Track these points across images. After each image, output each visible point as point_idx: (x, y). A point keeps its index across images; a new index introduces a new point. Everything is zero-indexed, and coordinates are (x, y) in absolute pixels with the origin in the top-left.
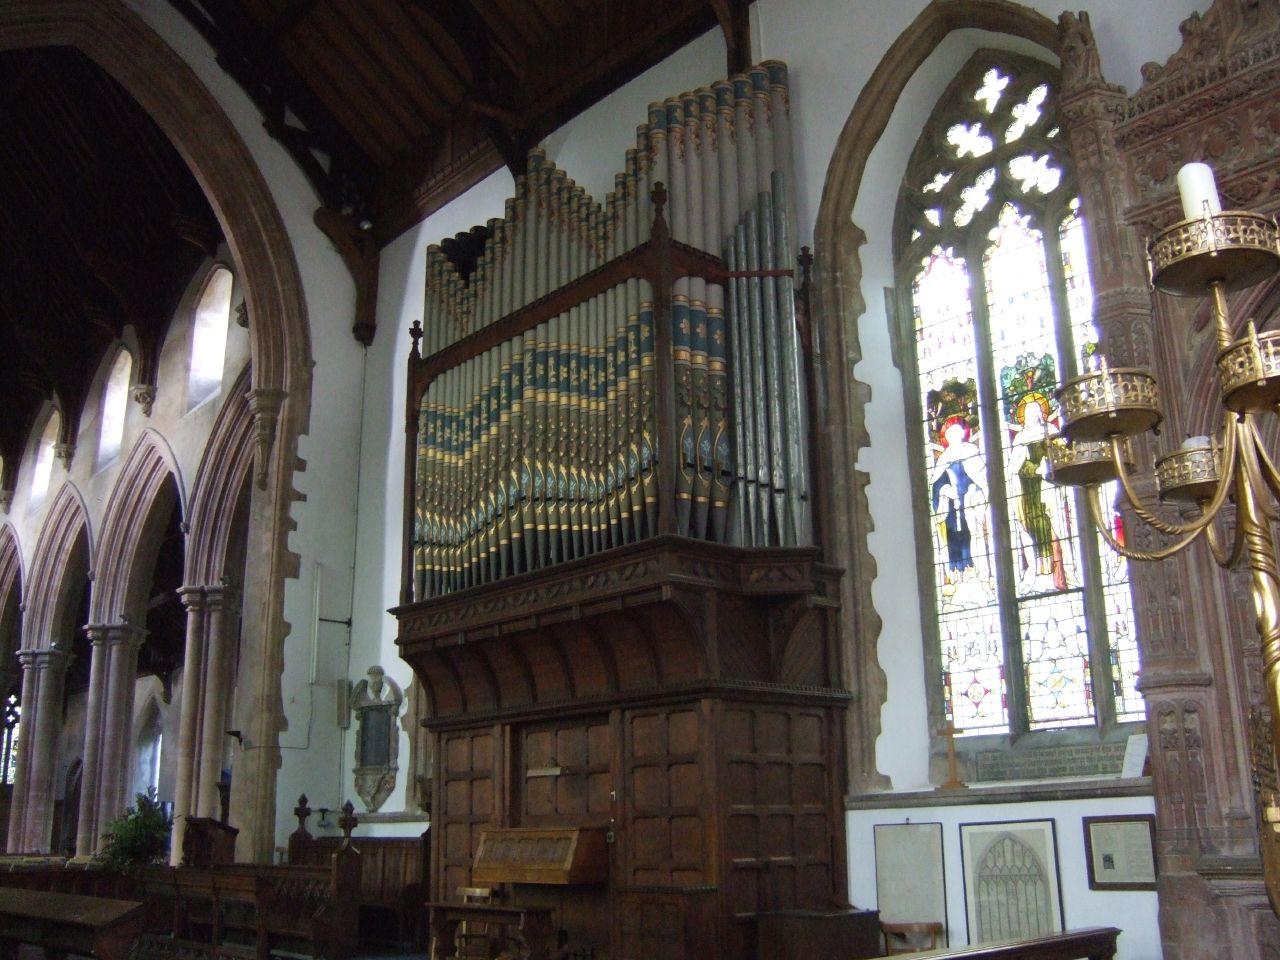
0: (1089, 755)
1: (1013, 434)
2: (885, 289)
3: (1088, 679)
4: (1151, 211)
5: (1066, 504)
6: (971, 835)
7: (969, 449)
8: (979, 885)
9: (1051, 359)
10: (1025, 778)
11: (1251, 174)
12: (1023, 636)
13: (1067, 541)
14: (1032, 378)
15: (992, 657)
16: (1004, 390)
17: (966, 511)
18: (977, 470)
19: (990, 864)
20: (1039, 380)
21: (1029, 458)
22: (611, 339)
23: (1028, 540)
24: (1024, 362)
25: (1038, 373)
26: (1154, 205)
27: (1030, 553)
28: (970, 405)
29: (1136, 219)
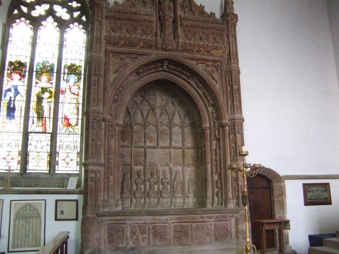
1: (37, 83)
2: (3, 23)
3: (49, 159)
4: (110, 38)
5: (50, 108)
6: (15, 204)
7: (20, 83)
8: (16, 220)
9: (54, 65)
10: (25, 187)
11: (138, 41)
12: (29, 144)
13: (48, 118)
14: (47, 69)
15: (16, 148)
16: (37, 69)
17: (15, 102)
18: (23, 90)
19: (21, 213)
20: (49, 70)
21: (41, 91)
23: (36, 115)
24: (45, 63)
25: (49, 68)
26: (112, 37)
27: (35, 119)
28: (24, 70)
29: (106, 39)
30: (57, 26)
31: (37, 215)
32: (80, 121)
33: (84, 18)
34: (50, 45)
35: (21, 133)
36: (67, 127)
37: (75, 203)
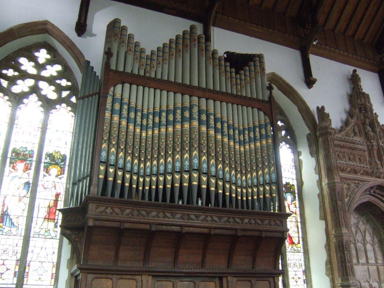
22: (145, 111)
30: (41, 106)
32: (301, 239)
33: (74, 99)
34: (63, 132)
36: (292, 245)
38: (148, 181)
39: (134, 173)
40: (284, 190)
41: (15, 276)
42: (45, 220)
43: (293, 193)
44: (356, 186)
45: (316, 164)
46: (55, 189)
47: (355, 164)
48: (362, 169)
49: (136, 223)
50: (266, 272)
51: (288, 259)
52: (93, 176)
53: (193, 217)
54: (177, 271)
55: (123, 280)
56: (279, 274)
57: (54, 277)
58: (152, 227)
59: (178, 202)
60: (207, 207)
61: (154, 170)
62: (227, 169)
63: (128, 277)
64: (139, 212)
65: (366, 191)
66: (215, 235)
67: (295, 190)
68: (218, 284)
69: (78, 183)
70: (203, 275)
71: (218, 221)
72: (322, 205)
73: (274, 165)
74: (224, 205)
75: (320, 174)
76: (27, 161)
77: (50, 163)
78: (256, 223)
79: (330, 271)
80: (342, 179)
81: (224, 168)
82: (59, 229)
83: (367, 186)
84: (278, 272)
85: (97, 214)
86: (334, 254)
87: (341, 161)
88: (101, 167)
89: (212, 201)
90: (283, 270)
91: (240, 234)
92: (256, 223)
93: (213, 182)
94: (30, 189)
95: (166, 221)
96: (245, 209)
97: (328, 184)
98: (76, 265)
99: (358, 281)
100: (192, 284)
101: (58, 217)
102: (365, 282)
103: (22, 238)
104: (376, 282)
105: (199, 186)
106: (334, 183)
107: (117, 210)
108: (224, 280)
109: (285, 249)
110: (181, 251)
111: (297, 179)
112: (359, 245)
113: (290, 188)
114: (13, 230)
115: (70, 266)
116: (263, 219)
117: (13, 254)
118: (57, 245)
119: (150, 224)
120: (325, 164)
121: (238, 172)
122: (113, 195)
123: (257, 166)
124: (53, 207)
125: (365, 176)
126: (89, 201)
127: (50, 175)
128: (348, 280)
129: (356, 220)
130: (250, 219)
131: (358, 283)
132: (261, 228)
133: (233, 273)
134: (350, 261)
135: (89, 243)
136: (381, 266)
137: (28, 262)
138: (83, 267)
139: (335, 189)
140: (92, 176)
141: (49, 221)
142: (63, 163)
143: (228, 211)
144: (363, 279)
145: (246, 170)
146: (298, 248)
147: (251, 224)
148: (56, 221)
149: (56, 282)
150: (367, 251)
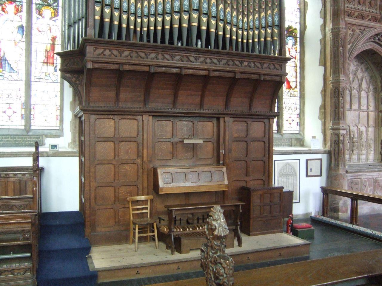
0: (23, 139)
6: (278, 163)
19: (283, 171)
31: (294, 173)
32: (298, 84)
35: (57, 83)
36: (289, 90)
37: (319, 161)
38: (146, 21)
39: (131, 14)
40: (286, 33)
41: (22, 118)
42: (44, 64)
43: (295, 37)
44: (361, 32)
45: (322, 7)
46: (51, 32)
47: (364, 8)
48: (370, 14)
49: (135, 65)
50: (263, 114)
51: (284, 103)
52: (88, 17)
53: (192, 59)
54: (177, 111)
55: (125, 120)
56: (274, 116)
57: (59, 119)
58: (151, 68)
59: (177, 44)
60: (206, 49)
61: (152, 9)
62: (228, 10)
63: (129, 117)
64: (138, 53)
65: (370, 38)
66: (214, 77)
67: (297, 34)
68: (215, 124)
69: (74, 24)
70: (202, 115)
71: (217, 63)
72: (323, 50)
73: (278, 7)
74: (224, 47)
75: (324, 17)
76: (17, 3)
77: (42, 5)
78: (255, 66)
79: (323, 115)
80: (347, 24)
81: (225, 9)
82: (59, 73)
83: (373, 33)
84: (273, 114)
85: (95, 56)
86: (329, 99)
87: (350, 5)
88: (96, 7)
89: (212, 42)
90: (278, 112)
91: (238, 76)
92: (255, 66)
93: (214, 24)
94: (25, 33)
95: (165, 63)
96: (245, 52)
97: (332, 29)
98: (79, 107)
99: (348, 125)
100: (191, 123)
101: (57, 60)
102: (354, 126)
103: (24, 82)
104: (364, 127)
105: (199, 27)
106: (339, 28)
107: (115, 52)
108: (222, 120)
109: (282, 93)
110: (181, 92)
111: (300, 23)
112: (354, 92)
113: (293, 32)
114: (14, 75)
115: (73, 108)
116: (262, 63)
117: (17, 98)
118: (58, 89)
119: (149, 66)
120: (331, 8)
121: (239, 13)
122: (110, 36)
123: (260, 7)
124: (51, 51)
125: (372, 22)
126: (86, 43)
127: (43, 17)
128: (338, 124)
129: (356, 67)
130: (250, 62)
131: (348, 127)
132: (260, 72)
133: (229, 114)
134: (343, 107)
135: (89, 85)
136: (371, 112)
137: (32, 106)
138: (85, 108)
139: (339, 35)
140: (87, 17)
141: (48, 65)
142: (56, 4)
143: (228, 54)
144: (352, 123)
145: (248, 11)
146: (293, 93)
147: (250, 67)
148: (55, 65)
149: (61, 123)
150: (360, 98)
